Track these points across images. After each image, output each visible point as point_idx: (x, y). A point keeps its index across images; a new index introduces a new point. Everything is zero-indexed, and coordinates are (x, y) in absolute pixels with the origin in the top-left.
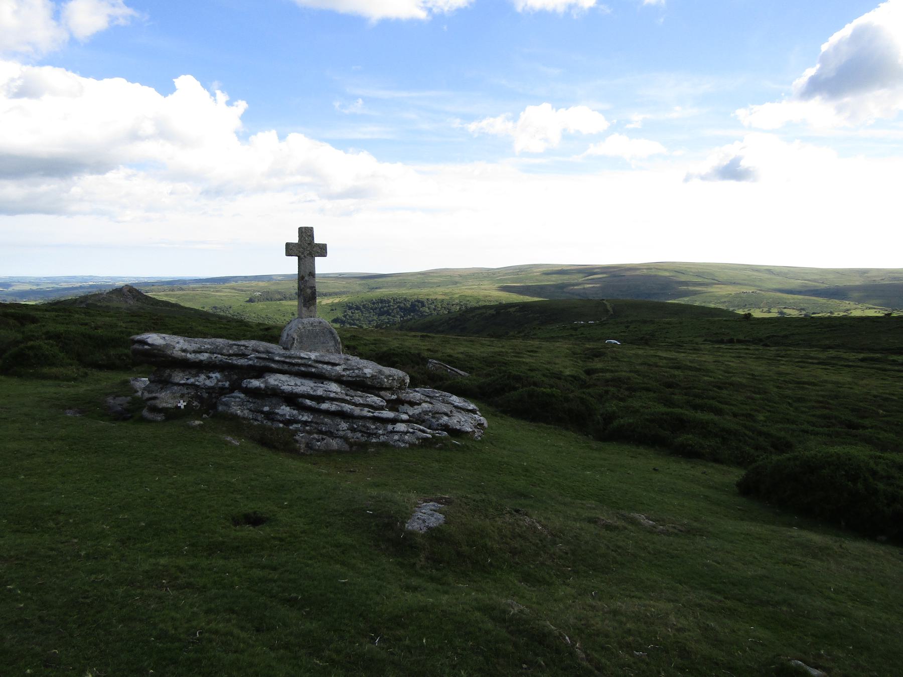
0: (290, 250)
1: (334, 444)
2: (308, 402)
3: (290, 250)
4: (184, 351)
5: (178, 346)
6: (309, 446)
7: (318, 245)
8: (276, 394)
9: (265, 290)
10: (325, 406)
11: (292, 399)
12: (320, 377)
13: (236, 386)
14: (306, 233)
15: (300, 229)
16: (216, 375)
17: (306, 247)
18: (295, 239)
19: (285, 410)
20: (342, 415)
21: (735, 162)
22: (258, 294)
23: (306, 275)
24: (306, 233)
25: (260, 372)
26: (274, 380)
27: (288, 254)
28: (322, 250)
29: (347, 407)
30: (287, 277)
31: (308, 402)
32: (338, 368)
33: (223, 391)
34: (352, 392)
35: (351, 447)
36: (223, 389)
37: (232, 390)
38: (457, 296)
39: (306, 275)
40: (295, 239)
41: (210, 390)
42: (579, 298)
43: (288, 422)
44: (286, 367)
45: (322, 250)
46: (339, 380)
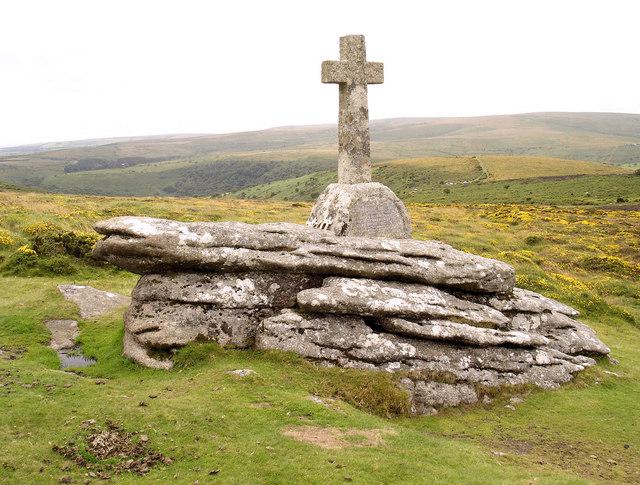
0: (328, 72)
1: (449, 393)
2: (410, 326)
4: (192, 245)
5: (183, 239)
6: (419, 400)
7: (371, 65)
8: (350, 314)
11: (379, 322)
14: (354, 46)
15: (341, 39)
16: (247, 283)
18: (334, 56)
19: (374, 342)
20: (459, 343)
21: (328, 72)
22: (76, 162)
23: (353, 117)
24: (354, 46)
25: (317, 277)
26: (348, 290)
27: (379, 68)
32: (440, 264)
33: (260, 312)
34: (461, 303)
35: (481, 396)
37: (276, 309)
38: (306, 157)
39: (353, 117)
40: (334, 56)
42: (615, 143)
43: (379, 362)
44: (361, 267)
45: (374, 74)
46: (442, 286)
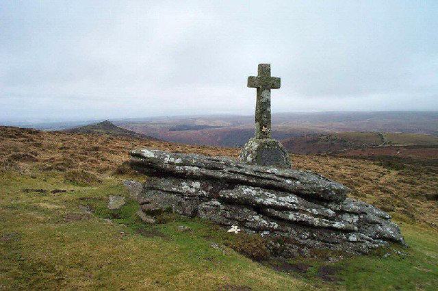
0: (251, 82)
2: (276, 213)
3: (251, 82)
5: (167, 160)
7: (274, 79)
8: (247, 203)
9: (232, 136)
10: (291, 216)
12: (283, 190)
13: (214, 195)
14: (264, 69)
16: (197, 184)
17: (264, 82)
18: (255, 74)
23: (263, 107)
24: (264, 69)
25: (232, 184)
26: (42, 218)
28: (276, 84)
29: (305, 217)
30: (250, 117)
31: (276, 213)
36: (202, 196)
39: (263, 107)
40: (255, 74)
41: (192, 196)
45: (276, 84)
46: (298, 193)
